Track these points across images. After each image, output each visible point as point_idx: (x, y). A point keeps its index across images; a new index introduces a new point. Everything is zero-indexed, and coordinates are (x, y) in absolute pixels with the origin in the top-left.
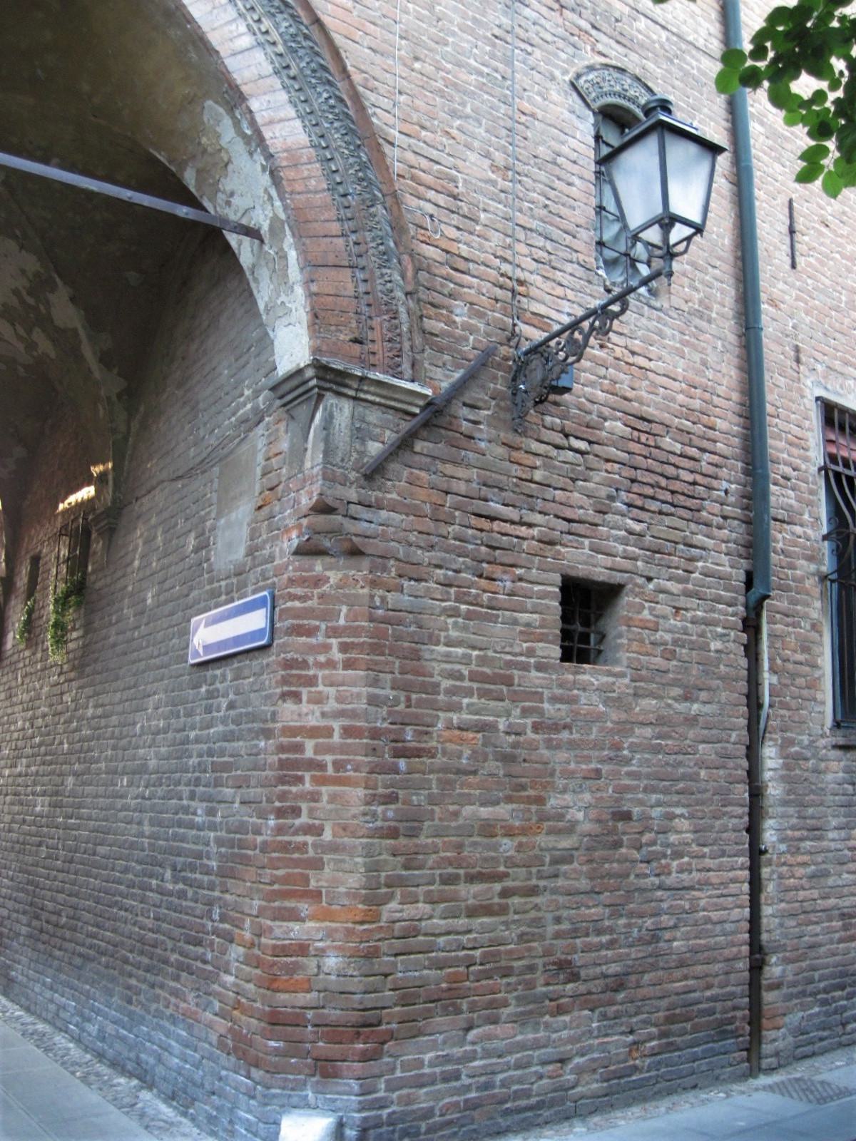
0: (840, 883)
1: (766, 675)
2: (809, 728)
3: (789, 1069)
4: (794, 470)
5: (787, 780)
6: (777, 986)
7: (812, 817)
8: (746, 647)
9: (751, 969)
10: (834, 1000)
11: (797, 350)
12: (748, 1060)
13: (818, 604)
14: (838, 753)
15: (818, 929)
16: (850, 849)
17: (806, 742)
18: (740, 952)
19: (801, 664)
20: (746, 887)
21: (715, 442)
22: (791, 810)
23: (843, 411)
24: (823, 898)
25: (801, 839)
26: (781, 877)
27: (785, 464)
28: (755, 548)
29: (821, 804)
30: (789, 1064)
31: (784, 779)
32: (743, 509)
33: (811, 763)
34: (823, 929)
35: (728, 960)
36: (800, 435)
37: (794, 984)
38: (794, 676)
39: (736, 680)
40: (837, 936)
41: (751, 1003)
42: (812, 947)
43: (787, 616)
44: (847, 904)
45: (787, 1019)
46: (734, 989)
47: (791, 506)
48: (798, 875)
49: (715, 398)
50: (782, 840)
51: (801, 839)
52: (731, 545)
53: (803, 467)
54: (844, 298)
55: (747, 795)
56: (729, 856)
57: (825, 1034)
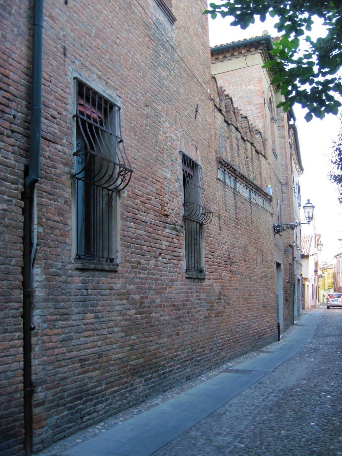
0: (79, 343)
1: (35, 227)
2: (61, 258)
3: (50, 449)
4: (59, 114)
5: (49, 288)
6: (42, 403)
7: (63, 308)
8: (23, 210)
9: (25, 397)
10: (76, 406)
11: (65, 49)
12: (24, 449)
13: (69, 190)
14: (79, 273)
15: (66, 369)
16: (84, 324)
17: (60, 266)
18: (17, 387)
19: (58, 222)
20: (21, 350)
21: (9, 85)
22: (50, 304)
23: (89, 89)
24: (69, 352)
25: (56, 320)
26: (44, 342)
27: (53, 109)
28: (31, 152)
29: (68, 300)
30: (50, 445)
31: (45, 286)
32: (24, 129)
33: (62, 278)
34: (69, 369)
35: (10, 393)
36: (63, 95)
37: (52, 401)
38: (53, 228)
39: (16, 228)
40: (78, 371)
41: (25, 416)
42: (63, 379)
43: (50, 194)
44: (82, 354)
45: (48, 421)
46: (14, 409)
47: (55, 133)
48: (54, 340)
49: (10, 60)
50: (45, 321)
51: (56, 320)
52: (16, 148)
53: (64, 113)
54: (94, 31)
55: (22, 296)
56: (10, 332)
57: (71, 425)
